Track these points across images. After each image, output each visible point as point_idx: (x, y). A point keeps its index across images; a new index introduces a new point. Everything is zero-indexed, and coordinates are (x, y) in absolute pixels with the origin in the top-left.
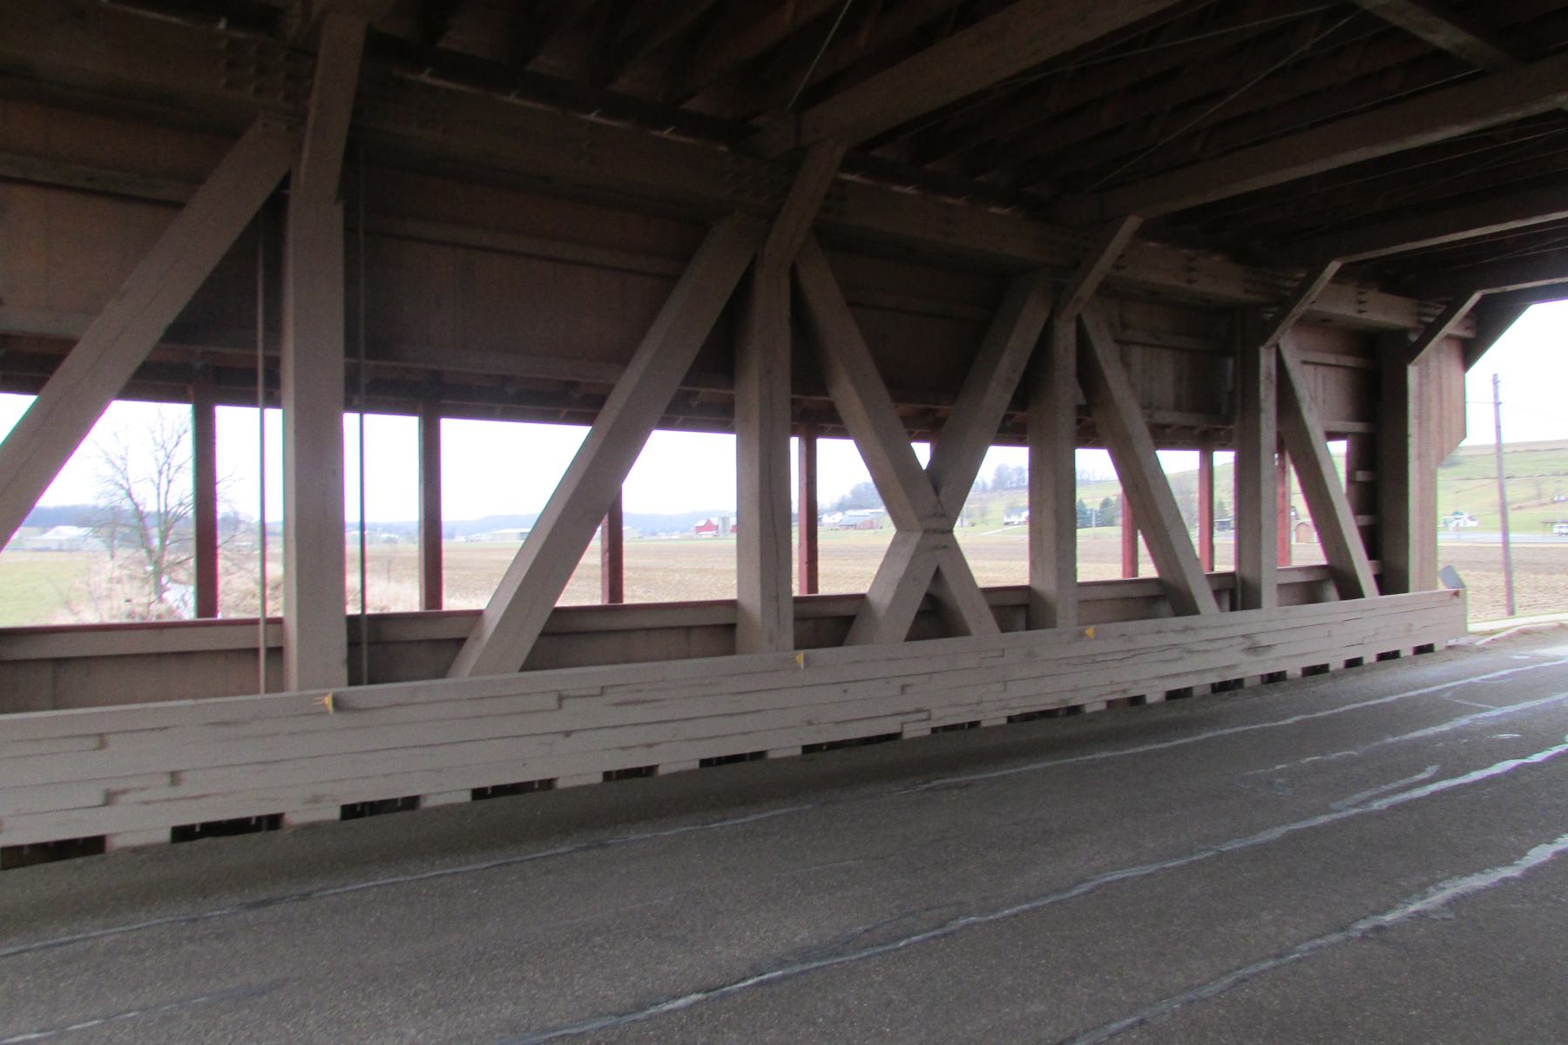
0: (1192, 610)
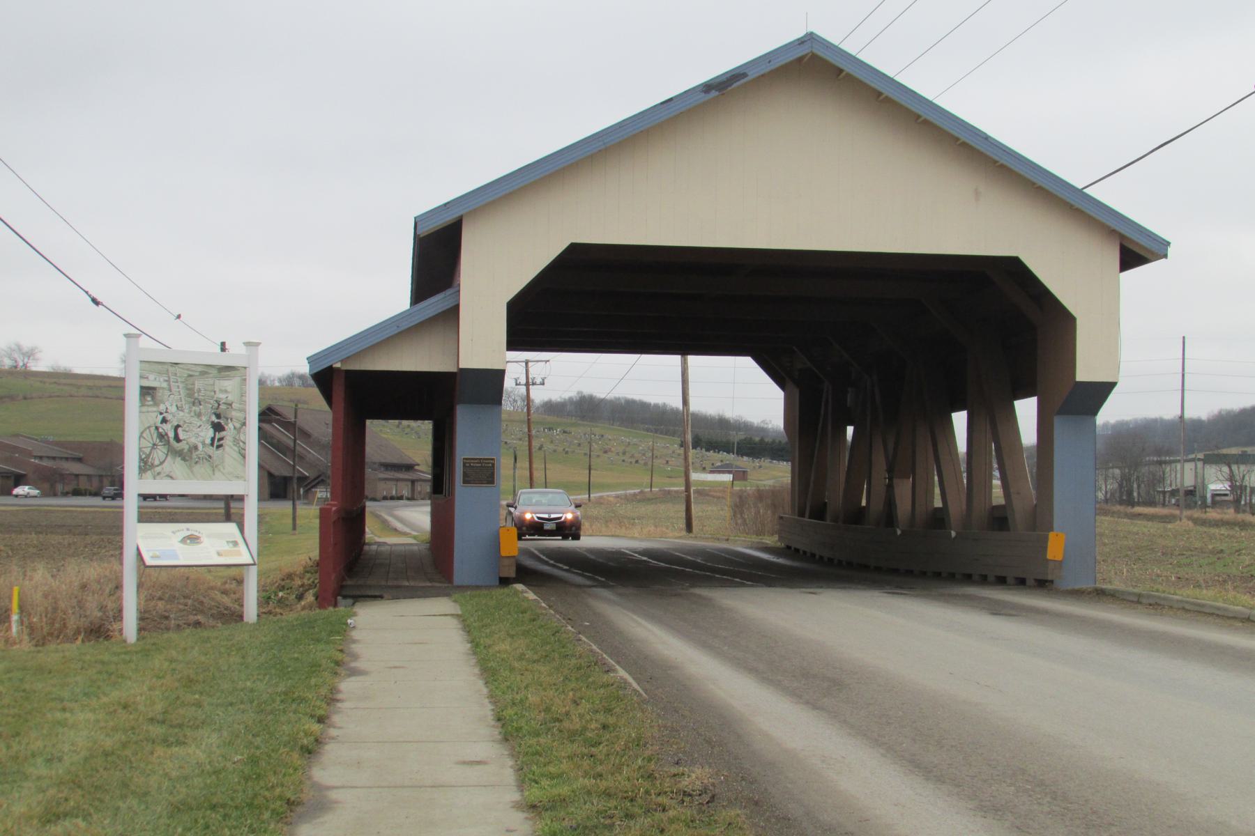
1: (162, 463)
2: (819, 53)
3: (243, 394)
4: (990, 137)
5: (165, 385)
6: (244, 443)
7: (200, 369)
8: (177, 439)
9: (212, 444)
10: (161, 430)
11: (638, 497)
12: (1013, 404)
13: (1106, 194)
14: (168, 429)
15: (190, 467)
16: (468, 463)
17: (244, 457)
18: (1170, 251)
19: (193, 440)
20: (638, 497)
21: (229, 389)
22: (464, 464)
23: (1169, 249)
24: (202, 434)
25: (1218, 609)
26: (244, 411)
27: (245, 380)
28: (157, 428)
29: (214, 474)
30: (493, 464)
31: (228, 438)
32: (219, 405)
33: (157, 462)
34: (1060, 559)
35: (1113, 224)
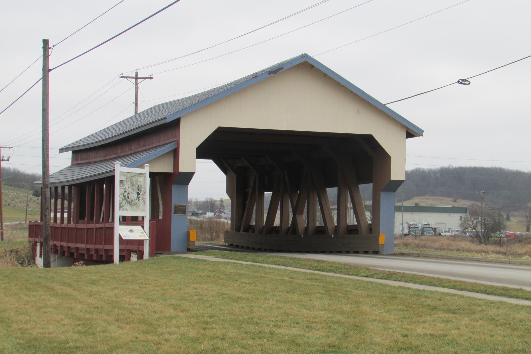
1: (124, 205)
2: (308, 61)
3: (145, 182)
4: (365, 92)
5: (125, 180)
6: (145, 199)
7: (134, 174)
8: (128, 198)
9: (137, 199)
10: (124, 195)
11: (19, 227)
12: (358, 186)
13: (397, 109)
14: (126, 194)
15: (131, 207)
17: (145, 204)
18: (424, 134)
19: (132, 198)
20: (19, 227)
21: (141, 181)
22: (175, 207)
23: (423, 133)
24: (134, 196)
25: (450, 256)
26: (145, 188)
27: (145, 178)
28: (123, 194)
29: (137, 209)
30: (185, 207)
31: (140, 197)
32: (139, 186)
33: (123, 205)
34: (383, 244)
35: (405, 124)
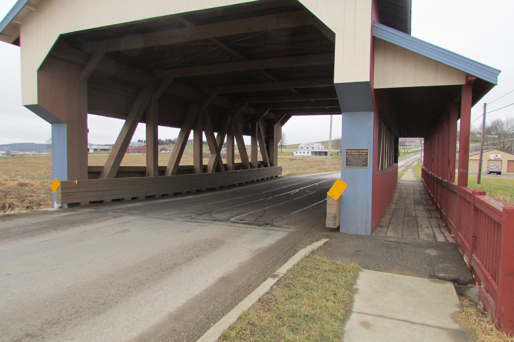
0: (267, 166)
16: (349, 152)
22: (347, 153)
